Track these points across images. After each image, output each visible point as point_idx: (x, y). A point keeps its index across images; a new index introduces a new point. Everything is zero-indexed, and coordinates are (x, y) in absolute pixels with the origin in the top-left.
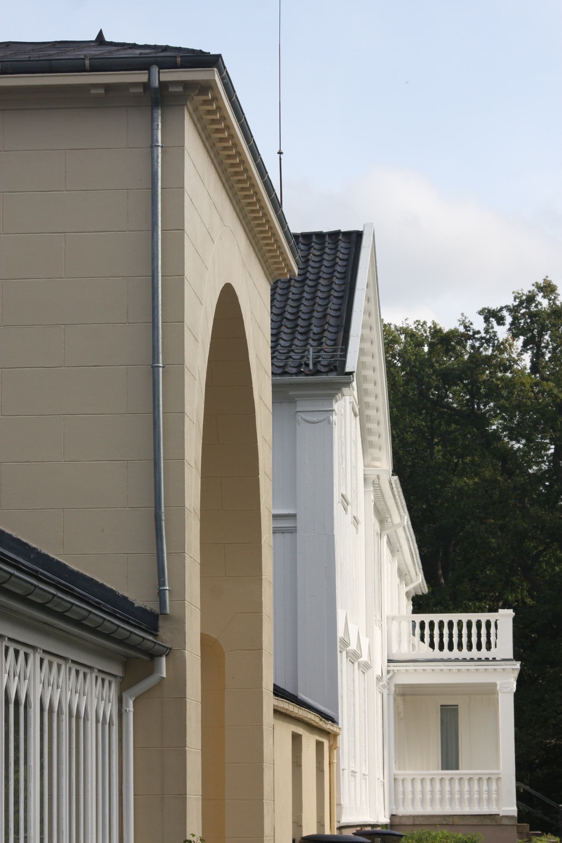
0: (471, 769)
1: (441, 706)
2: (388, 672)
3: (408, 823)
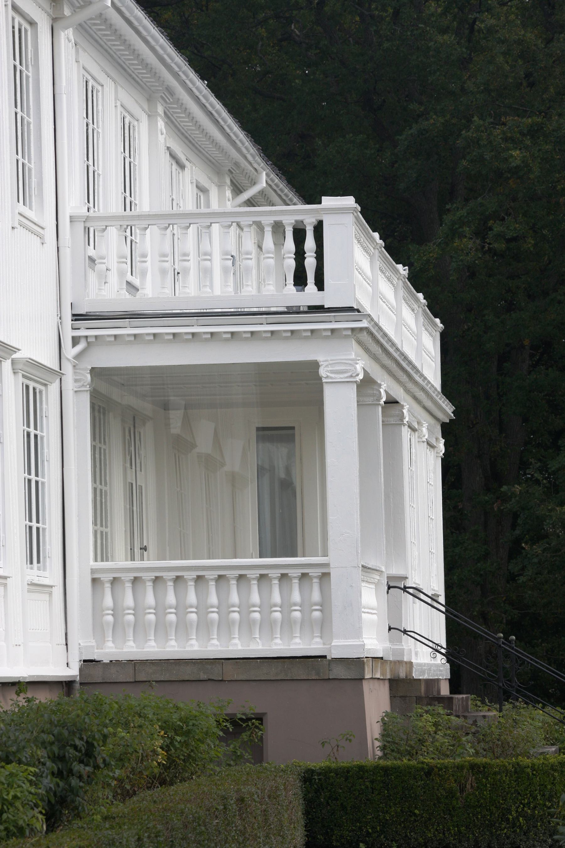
0: (235, 557)
2: (75, 341)
3: (121, 679)
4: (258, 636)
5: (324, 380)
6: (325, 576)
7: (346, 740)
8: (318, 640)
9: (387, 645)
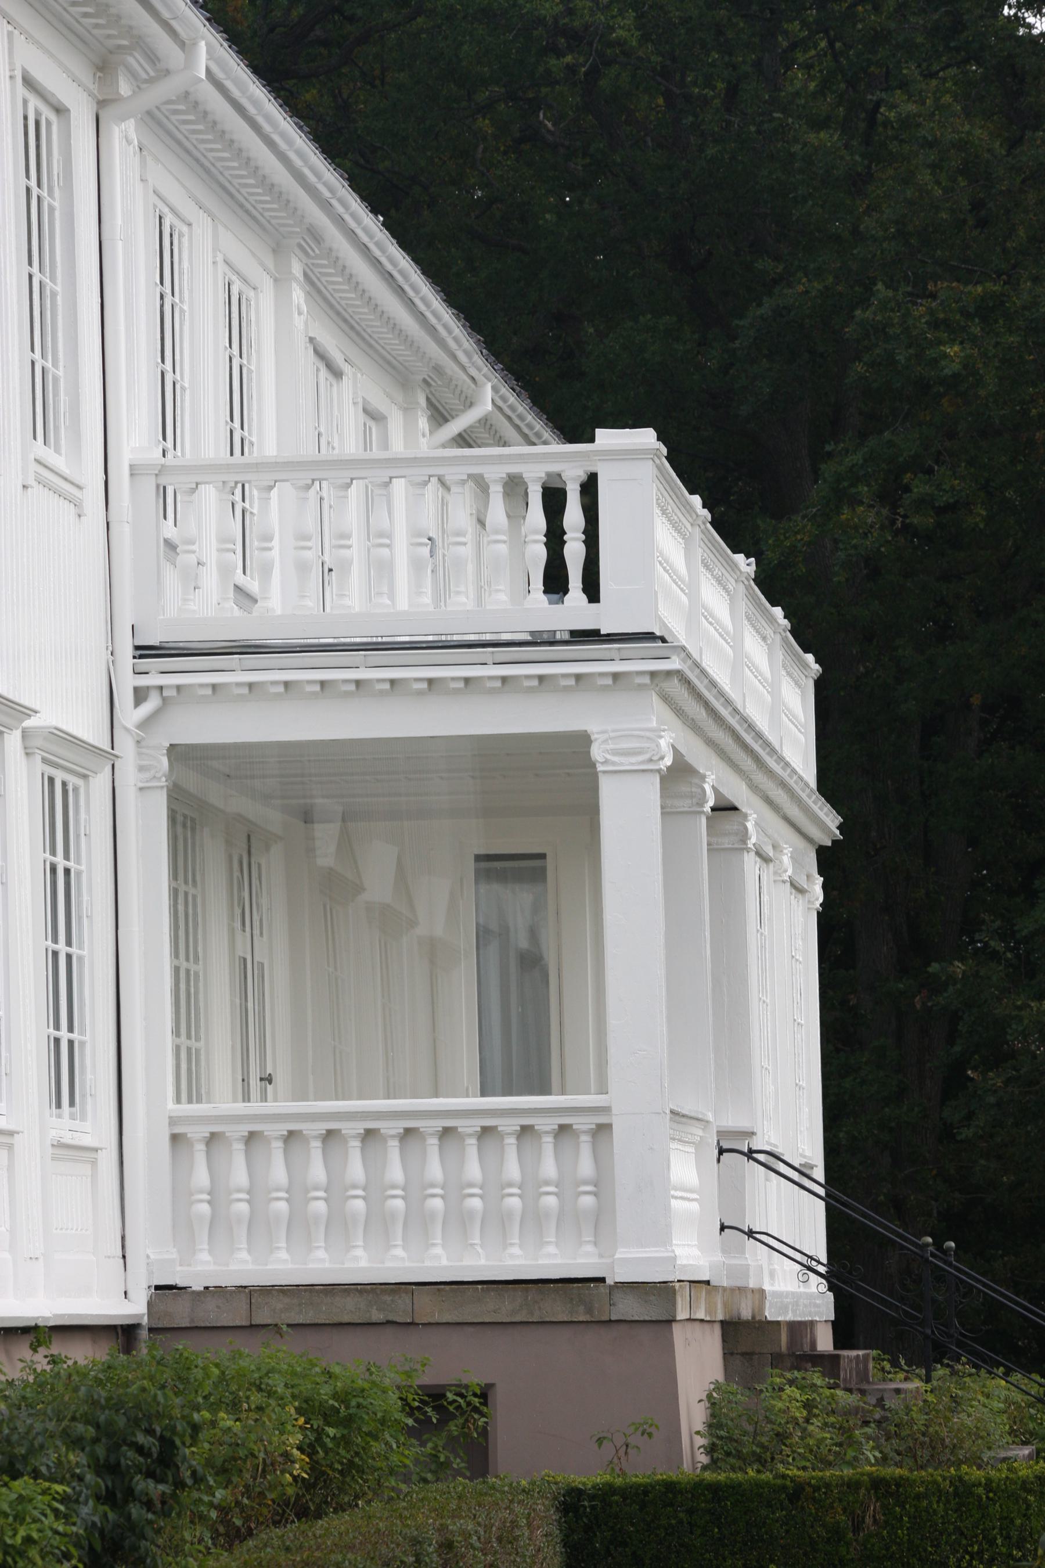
0: (436, 1095)
1: (478, 858)
2: (140, 695)
4: (477, 1241)
5: (600, 768)
6: (603, 1130)
7: (643, 1434)
8: (590, 1248)
9: (719, 1257)
